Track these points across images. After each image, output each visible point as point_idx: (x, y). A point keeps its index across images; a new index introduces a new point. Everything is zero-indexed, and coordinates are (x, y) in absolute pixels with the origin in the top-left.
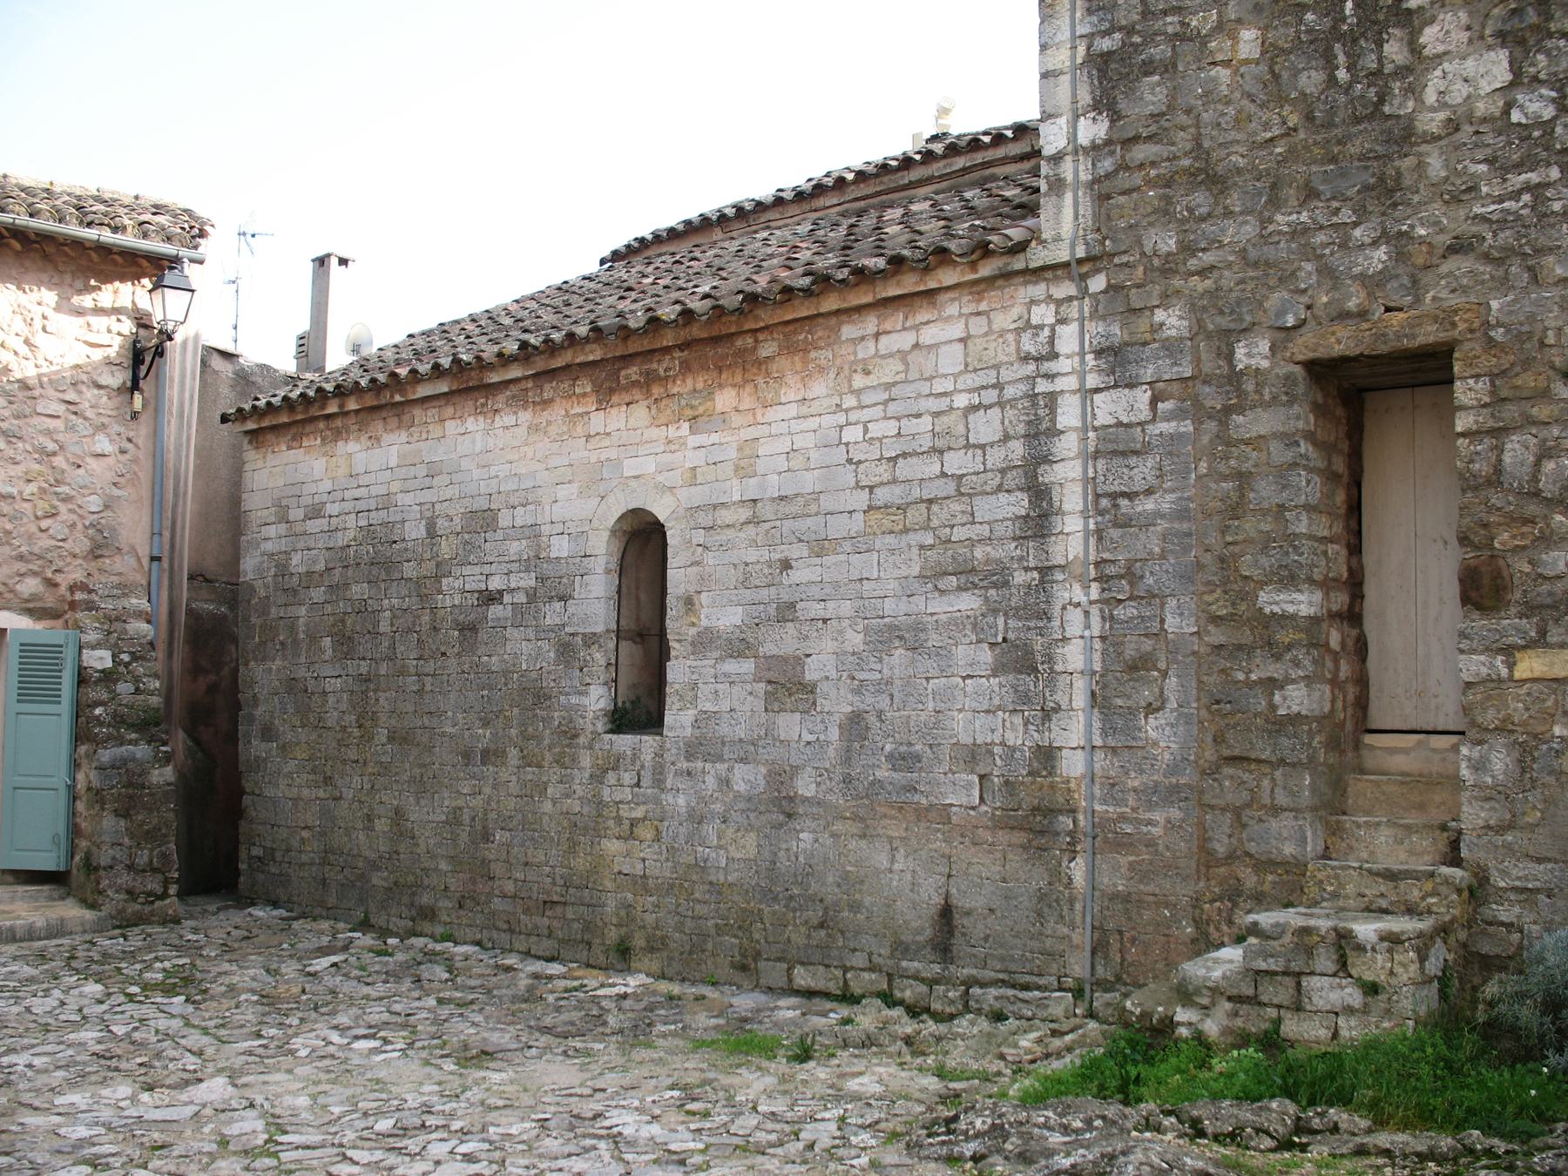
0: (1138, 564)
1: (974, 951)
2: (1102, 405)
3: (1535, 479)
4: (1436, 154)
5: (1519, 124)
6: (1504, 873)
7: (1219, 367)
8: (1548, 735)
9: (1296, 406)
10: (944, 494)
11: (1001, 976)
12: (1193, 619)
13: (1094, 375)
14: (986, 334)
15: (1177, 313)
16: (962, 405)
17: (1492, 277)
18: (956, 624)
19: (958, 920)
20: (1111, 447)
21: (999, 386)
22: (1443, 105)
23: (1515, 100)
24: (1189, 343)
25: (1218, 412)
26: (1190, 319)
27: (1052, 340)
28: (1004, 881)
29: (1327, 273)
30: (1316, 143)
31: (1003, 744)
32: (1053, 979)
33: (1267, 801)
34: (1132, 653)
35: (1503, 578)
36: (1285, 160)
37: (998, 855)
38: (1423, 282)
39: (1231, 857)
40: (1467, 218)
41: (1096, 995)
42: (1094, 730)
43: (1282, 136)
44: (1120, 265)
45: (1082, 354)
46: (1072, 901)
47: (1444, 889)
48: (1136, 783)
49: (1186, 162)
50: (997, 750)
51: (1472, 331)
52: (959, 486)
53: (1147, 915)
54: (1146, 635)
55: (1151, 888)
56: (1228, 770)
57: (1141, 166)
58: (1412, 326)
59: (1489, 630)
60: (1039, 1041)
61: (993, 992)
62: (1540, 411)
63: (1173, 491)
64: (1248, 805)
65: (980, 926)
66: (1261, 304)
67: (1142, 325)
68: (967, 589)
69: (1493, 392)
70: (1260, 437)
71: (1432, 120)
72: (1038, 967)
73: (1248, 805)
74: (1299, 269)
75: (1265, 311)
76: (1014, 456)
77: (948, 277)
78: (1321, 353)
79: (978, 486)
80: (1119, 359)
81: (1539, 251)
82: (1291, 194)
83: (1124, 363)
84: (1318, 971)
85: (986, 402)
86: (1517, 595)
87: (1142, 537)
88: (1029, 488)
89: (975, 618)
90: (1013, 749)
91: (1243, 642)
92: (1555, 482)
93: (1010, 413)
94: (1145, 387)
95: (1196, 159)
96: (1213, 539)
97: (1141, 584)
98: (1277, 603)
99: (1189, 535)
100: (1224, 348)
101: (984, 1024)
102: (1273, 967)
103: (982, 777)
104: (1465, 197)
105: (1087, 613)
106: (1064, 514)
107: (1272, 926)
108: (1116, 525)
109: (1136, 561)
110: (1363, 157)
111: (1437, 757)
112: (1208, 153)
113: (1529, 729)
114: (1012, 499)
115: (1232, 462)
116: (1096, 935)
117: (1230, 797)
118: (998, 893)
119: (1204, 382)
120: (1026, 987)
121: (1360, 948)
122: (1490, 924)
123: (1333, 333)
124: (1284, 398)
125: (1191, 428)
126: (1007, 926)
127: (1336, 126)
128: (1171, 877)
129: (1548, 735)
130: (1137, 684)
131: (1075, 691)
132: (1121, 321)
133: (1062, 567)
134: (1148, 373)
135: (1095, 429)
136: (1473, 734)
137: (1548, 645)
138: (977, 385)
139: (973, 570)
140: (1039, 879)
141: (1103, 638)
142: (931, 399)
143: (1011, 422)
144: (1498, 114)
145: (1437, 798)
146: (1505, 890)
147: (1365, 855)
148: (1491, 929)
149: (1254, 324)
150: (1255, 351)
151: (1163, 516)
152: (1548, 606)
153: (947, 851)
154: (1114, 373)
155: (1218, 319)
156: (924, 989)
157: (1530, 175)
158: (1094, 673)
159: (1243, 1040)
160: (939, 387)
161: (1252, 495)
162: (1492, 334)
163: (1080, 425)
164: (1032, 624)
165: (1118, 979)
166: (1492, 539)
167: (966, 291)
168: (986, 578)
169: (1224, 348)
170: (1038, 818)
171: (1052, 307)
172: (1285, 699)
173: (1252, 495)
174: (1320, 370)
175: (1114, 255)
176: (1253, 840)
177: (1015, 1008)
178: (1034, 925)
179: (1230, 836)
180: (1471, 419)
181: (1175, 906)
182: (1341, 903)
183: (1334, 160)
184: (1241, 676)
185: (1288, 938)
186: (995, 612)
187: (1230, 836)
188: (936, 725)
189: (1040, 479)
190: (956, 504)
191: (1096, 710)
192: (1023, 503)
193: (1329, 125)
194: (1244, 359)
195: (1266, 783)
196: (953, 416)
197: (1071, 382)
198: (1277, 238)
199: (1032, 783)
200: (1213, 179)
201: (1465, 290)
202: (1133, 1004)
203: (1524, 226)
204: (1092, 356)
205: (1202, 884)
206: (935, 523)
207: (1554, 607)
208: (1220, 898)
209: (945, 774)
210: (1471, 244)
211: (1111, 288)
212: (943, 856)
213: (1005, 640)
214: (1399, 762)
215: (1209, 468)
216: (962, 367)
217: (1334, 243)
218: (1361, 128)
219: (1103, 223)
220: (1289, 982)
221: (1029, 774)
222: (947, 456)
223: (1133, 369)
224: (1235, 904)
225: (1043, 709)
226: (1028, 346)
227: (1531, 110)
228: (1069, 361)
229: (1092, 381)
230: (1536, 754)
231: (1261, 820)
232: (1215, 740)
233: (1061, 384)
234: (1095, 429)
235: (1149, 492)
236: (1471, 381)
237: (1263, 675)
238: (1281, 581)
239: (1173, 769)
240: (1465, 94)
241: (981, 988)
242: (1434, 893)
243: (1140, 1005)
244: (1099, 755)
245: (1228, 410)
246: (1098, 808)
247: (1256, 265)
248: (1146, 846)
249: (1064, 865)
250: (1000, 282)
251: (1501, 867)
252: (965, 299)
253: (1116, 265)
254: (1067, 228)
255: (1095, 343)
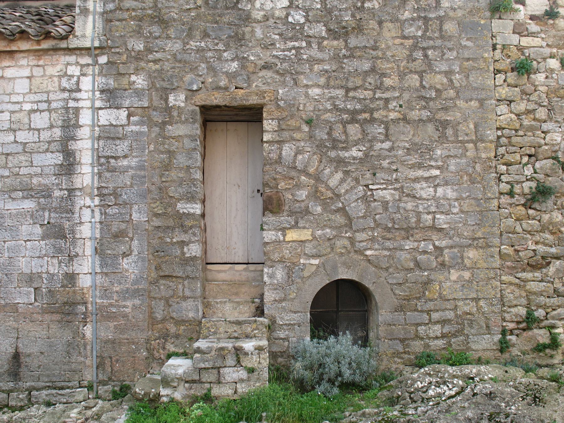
0: (119, 189)
1: (33, 373)
2: (102, 115)
3: (294, 162)
4: (259, 28)
5: (291, 23)
6: (282, 318)
7: (161, 104)
8: (298, 263)
9: (196, 124)
10: (16, 151)
11: (48, 384)
12: (146, 215)
13: (100, 102)
14: (42, 76)
15: (142, 78)
16: (27, 109)
17: (280, 80)
18: (22, 215)
19: (23, 359)
20: (106, 135)
21: (48, 102)
22: (263, 9)
23: (290, 13)
24: (147, 92)
25: (160, 123)
26: (148, 81)
27: (78, 83)
28: (48, 338)
29: (211, 69)
30: (209, 14)
31: (47, 273)
32: (76, 383)
33: (181, 294)
34: (116, 230)
35: (281, 201)
36: (195, 19)
37: (45, 326)
38: (251, 79)
39: (164, 320)
40: (271, 55)
41: (100, 387)
42: (96, 265)
43: (194, 8)
44: (115, 53)
45: (93, 91)
46: (85, 346)
47: (260, 327)
48: (118, 289)
49: (150, 12)
50: (44, 276)
51: (271, 101)
52: (24, 148)
53: (124, 349)
54: (122, 222)
55: (126, 336)
56: (162, 282)
57: (128, 10)
58: (247, 96)
59: (276, 221)
60: (80, 413)
61: (45, 392)
62: (297, 135)
63: (137, 157)
64: (172, 297)
65: (36, 361)
66: (182, 79)
67: (124, 81)
68: (28, 198)
69: (279, 126)
70: (179, 136)
71: (258, 14)
72: (68, 378)
73: (172, 297)
74: (199, 66)
75: (183, 82)
76: (56, 135)
77: (24, 45)
78: (208, 103)
79: (35, 148)
80: (112, 95)
81: (297, 73)
82: (197, 34)
83: (115, 98)
84: (228, 365)
85: (41, 108)
86: (287, 208)
87: (121, 177)
88: (63, 151)
89: (33, 212)
90: (53, 275)
91: (170, 225)
92: (302, 164)
93: (54, 115)
94: (124, 109)
95: (155, 11)
96: (156, 179)
97: (120, 199)
98: (186, 208)
99: (145, 177)
100: (164, 96)
101: (43, 408)
102: (208, 366)
103: (35, 289)
104: (270, 47)
105: (93, 211)
106: (81, 164)
107: (206, 348)
108: (108, 171)
109: (118, 188)
110: (229, 24)
111: (238, 273)
112: (160, 10)
113: (291, 261)
114: (54, 156)
115: (166, 146)
116: (99, 360)
117: (163, 294)
118: (46, 344)
119: (154, 110)
120: (62, 388)
121: (246, 354)
122: (276, 339)
123: (214, 95)
124: (191, 120)
125: (147, 130)
126: (50, 360)
127: (218, 9)
128: (135, 330)
129: (298, 263)
130: (118, 244)
131: (86, 247)
132: (114, 78)
133: (80, 189)
134: (127, 103)
135: (99, 126)
136: (268, 263)
137: (300, 228)
138: (36, 100)
139: (31, 189)
140: (68, 336)
141: (101, 223)
142: (10, 104)
143: (54, 119)
144: (283, 17)
145: (243, 290)
146: (282, 325)
147: (220, 315)
148: (277, 341)
149: (178, 87)
150: (178, 98)
151: (132, 168)
152: (299, 212)
153: (16, 326)
154: (109, 101)
155: (162, 83)
156: (5, 395)
157: (295, 43)
158: (96, 239)
159: (195, 400)
160: (14, 99)
161: (175, 161)
162: (279, 103)
163: (91, 124)
164: (64, 216)
165: (110, 379)
166: (278, 185)
167: (32, 54)
168: (38, 193)
169: (164, 96)
170: (67, 307)
171: (79, 68)
172: (189, 250)
173: (175, 161)
174: (205, 109)
175: (112, 48)
176: (175, 312)
177: (57, 399)
178: (65, 358)
179: (163, 311)
180: (270, 136)
181: (137, 343)
182: (218, 336)
183: (217, 22)
184: (168, 240)
185: (213, 353)
186: (44, 209)
187: (163, 311)
188: (10, 264)
189: (70, 147)
190: (23, 157)
191: (97, 256)
192: (60, 158)
193: (215, 8)
194: (173, 101)
195: (180, 286)
196: (22, 114)
197: (88, 104)
198: (190, 52)
199: (63, 291)
200: (164, 23)
201: (268, 84)
202: (139, 390)
203: (292, 62)
204: (99, 92)
205: (150, 333)
206: (10, 165)
207: (301, 213)
208: (159, 338)
209: (15, 288)
210: (272, 66)
211: (109, 62)
212: (14, 329)
213: (49, 223)
214: (222, 276)
215: (155, 148)
216: (28, 91)
217: (215, 57)
218: (229, 11)
219: (107, 31)
220: (215, 371)
221: (62, 286)
222: (18, 133)
223: (119, 101)
224: (166, 340)
225: (69, 256)
226: (65, 84)
227: (296, 18)
228: (87, 94)
229: (98, 104)
230: (294, 271)
231: (178, 303)
232: (156, 268)
233: (81, 104)
234: (99, 126)
235: (125, 157)
236: (270, 121)
237: (179, 240)
238: (187, 199)
239: (136, 282)
240: (271, 7)
241: (37, 391)
242: (257, 329)
243: (143, 390)
244: (99, 277)
245: (164, 123)
246: (98, 301)
247: (180, 61)
248: (123, 317)
249: (81, 329)
250: (51, 52)
251: (281, 316)
252: (31, 58)
253: (113, 53)
254: (89, 31)
255: (100, 87)
